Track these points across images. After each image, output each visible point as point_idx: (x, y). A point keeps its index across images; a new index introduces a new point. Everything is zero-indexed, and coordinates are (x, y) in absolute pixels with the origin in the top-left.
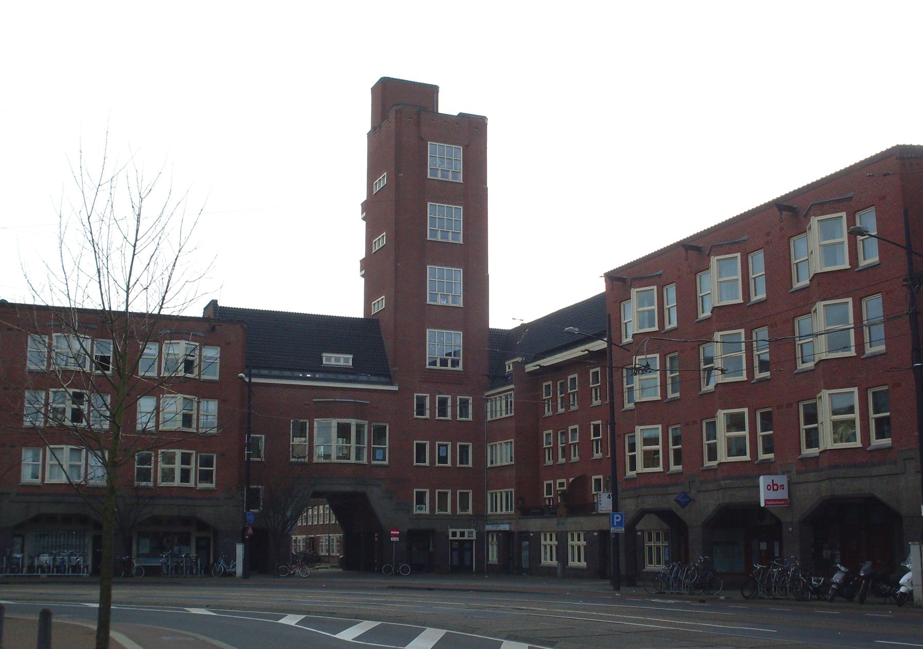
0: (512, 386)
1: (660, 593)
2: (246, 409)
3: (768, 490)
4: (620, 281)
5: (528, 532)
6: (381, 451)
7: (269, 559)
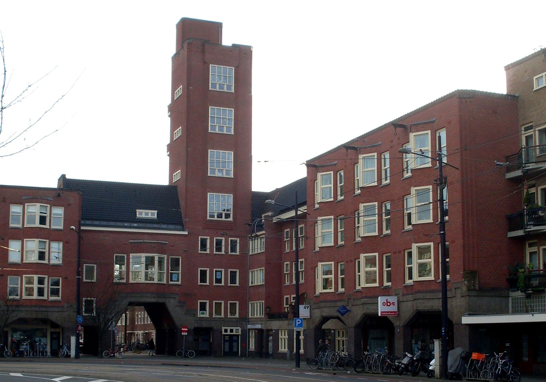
0: (264, 232)
1: (318, 369)
2: (80, 248)
3: (383, 306)
4: (314, 166)
5: (272, 330)
6: (176, 275)
7: (96, 344)
